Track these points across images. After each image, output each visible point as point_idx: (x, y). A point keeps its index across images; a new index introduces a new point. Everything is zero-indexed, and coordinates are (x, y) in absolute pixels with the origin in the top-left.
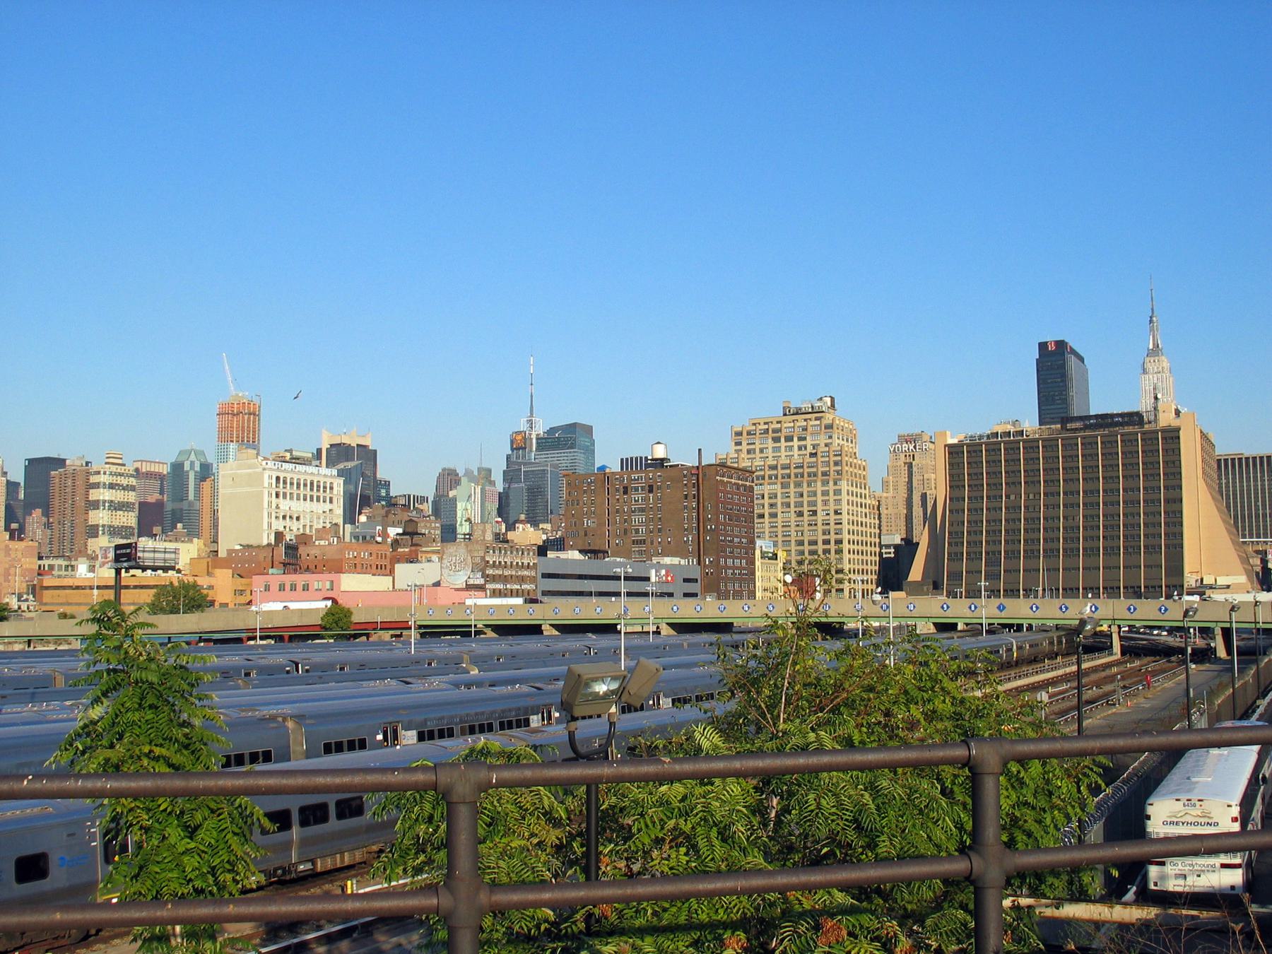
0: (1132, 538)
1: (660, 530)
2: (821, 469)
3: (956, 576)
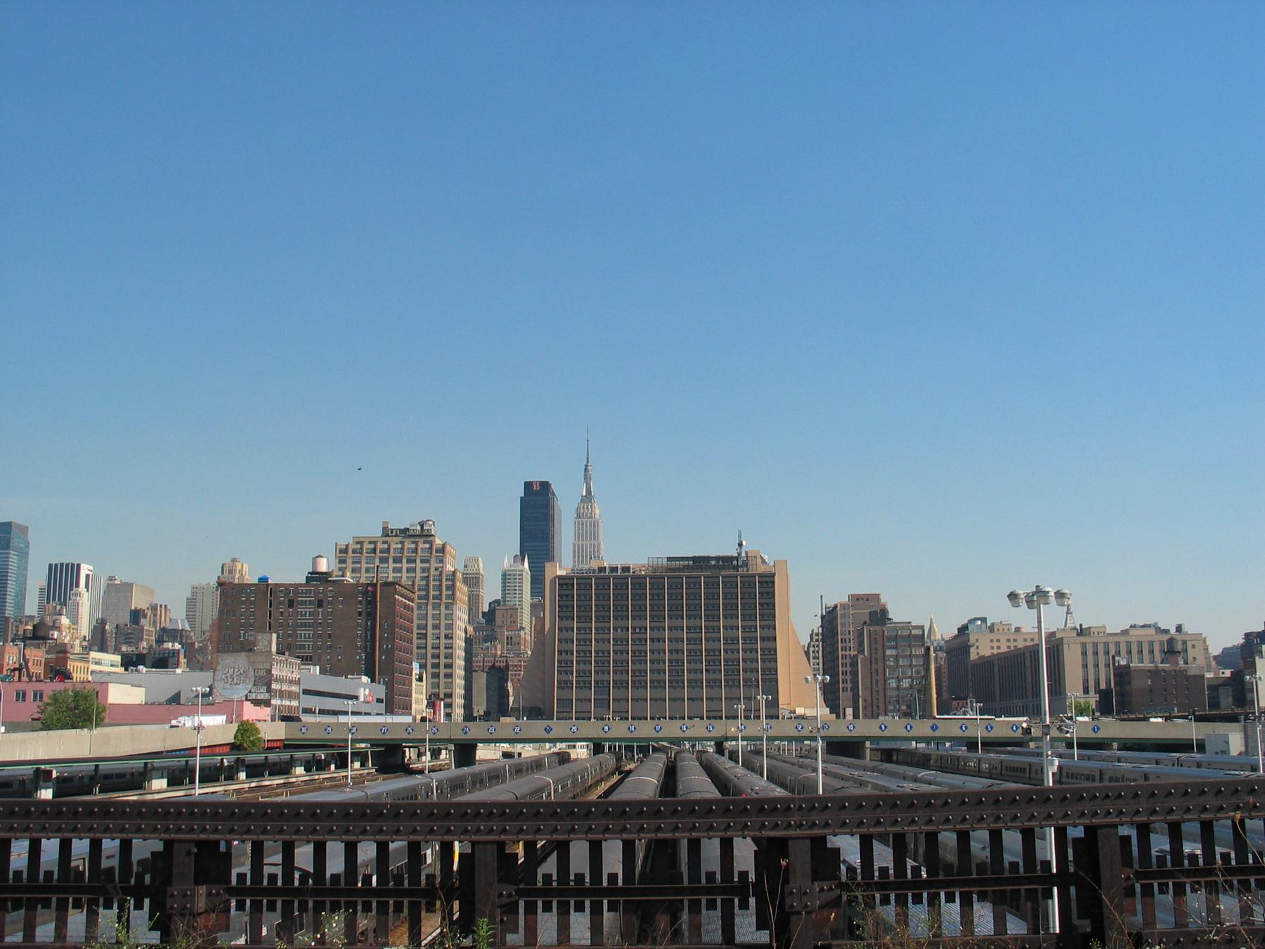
1: (330, 647)
3: (565, 702)
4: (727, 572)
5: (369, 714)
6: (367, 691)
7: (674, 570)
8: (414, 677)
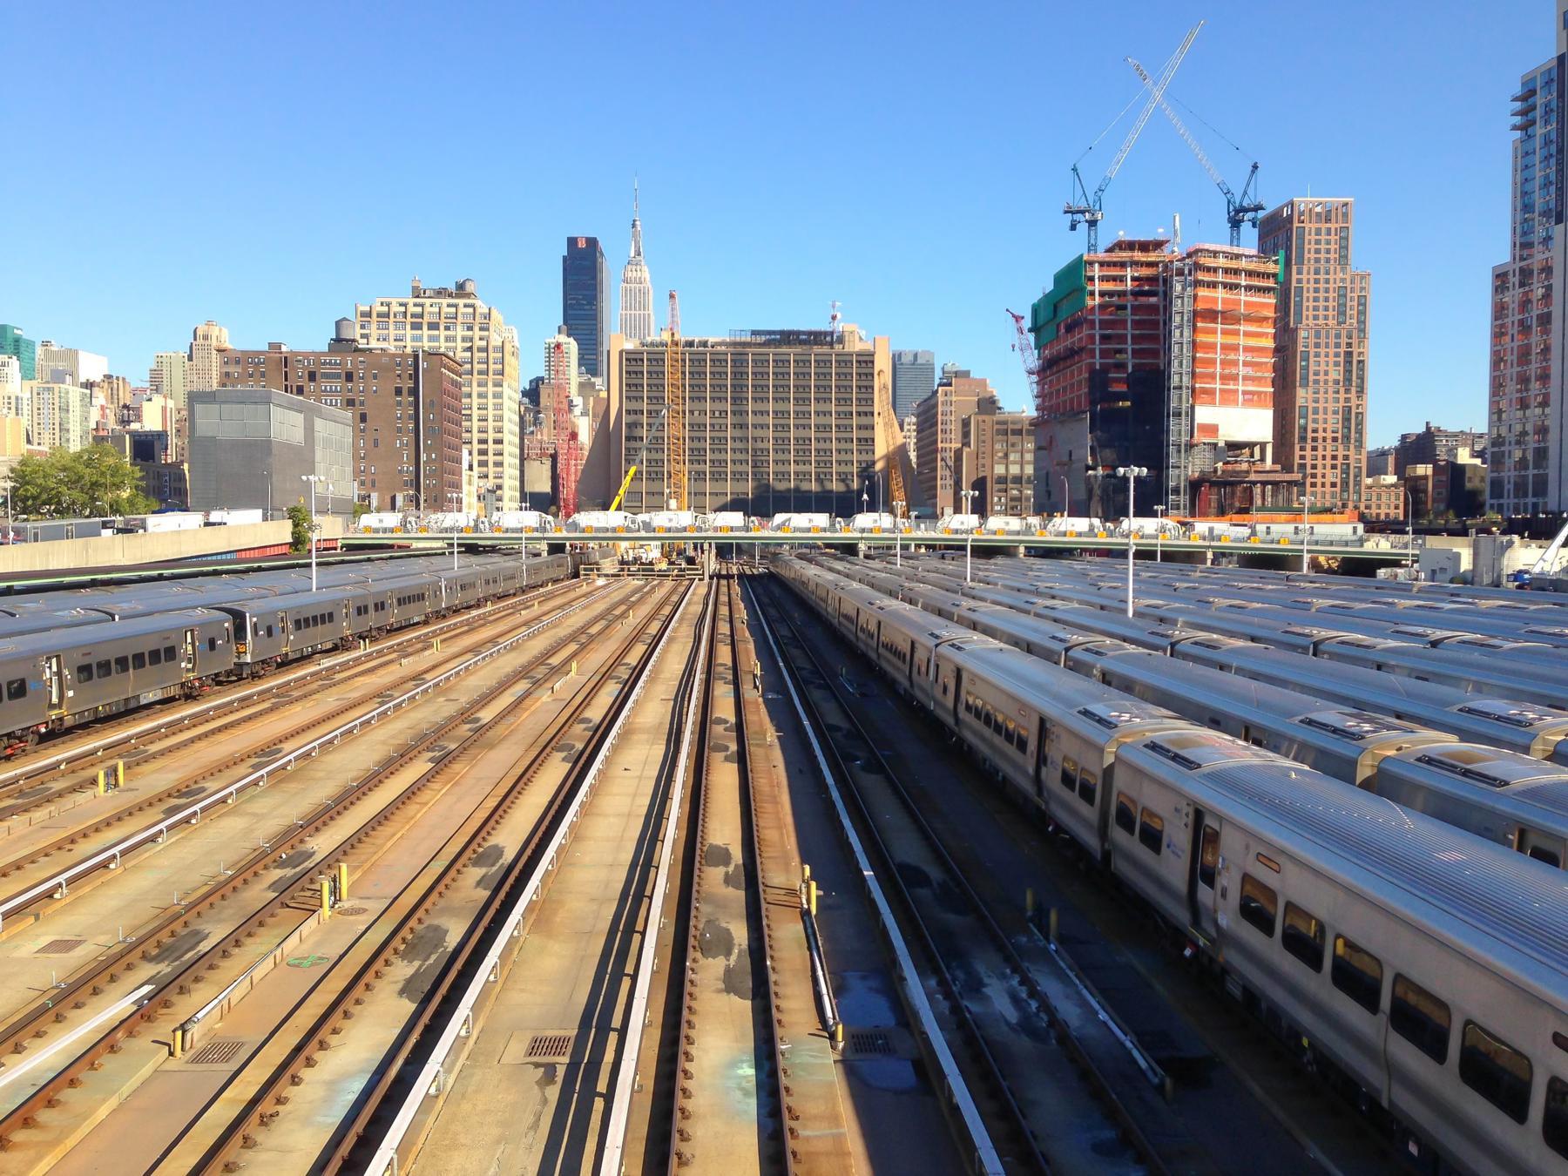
8: (465, 465)
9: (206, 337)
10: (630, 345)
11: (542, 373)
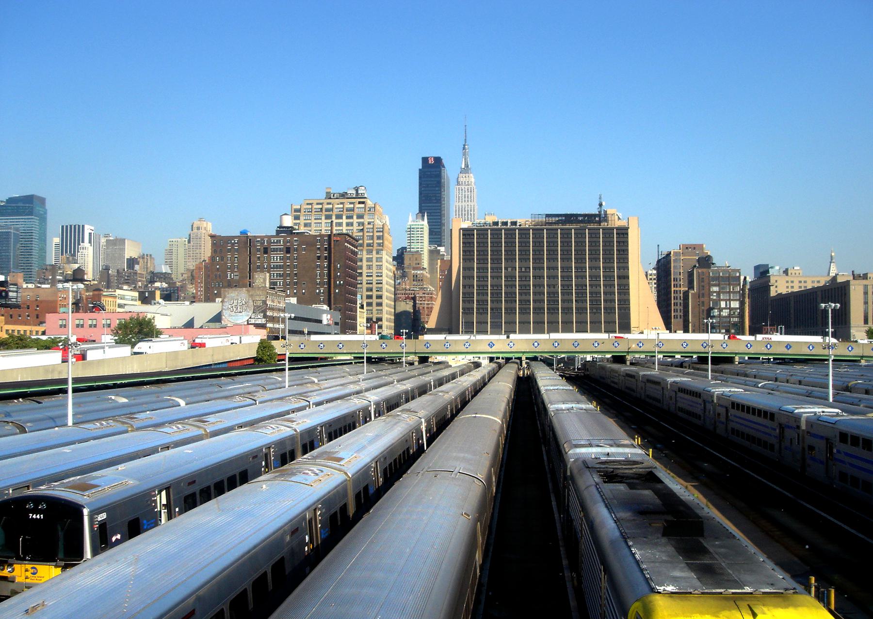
0: (595, 302)
1: (296, 283)
2: (366, 242)
4: (592, 226)
5: (329, 334)
6: (329, 316)
7: (551, 224)
9: (198, 228)
10: (466, 225)
11: (406, 245)
